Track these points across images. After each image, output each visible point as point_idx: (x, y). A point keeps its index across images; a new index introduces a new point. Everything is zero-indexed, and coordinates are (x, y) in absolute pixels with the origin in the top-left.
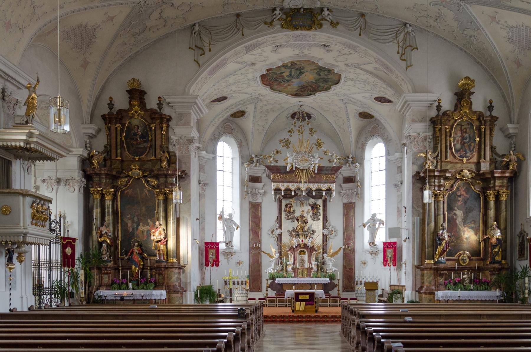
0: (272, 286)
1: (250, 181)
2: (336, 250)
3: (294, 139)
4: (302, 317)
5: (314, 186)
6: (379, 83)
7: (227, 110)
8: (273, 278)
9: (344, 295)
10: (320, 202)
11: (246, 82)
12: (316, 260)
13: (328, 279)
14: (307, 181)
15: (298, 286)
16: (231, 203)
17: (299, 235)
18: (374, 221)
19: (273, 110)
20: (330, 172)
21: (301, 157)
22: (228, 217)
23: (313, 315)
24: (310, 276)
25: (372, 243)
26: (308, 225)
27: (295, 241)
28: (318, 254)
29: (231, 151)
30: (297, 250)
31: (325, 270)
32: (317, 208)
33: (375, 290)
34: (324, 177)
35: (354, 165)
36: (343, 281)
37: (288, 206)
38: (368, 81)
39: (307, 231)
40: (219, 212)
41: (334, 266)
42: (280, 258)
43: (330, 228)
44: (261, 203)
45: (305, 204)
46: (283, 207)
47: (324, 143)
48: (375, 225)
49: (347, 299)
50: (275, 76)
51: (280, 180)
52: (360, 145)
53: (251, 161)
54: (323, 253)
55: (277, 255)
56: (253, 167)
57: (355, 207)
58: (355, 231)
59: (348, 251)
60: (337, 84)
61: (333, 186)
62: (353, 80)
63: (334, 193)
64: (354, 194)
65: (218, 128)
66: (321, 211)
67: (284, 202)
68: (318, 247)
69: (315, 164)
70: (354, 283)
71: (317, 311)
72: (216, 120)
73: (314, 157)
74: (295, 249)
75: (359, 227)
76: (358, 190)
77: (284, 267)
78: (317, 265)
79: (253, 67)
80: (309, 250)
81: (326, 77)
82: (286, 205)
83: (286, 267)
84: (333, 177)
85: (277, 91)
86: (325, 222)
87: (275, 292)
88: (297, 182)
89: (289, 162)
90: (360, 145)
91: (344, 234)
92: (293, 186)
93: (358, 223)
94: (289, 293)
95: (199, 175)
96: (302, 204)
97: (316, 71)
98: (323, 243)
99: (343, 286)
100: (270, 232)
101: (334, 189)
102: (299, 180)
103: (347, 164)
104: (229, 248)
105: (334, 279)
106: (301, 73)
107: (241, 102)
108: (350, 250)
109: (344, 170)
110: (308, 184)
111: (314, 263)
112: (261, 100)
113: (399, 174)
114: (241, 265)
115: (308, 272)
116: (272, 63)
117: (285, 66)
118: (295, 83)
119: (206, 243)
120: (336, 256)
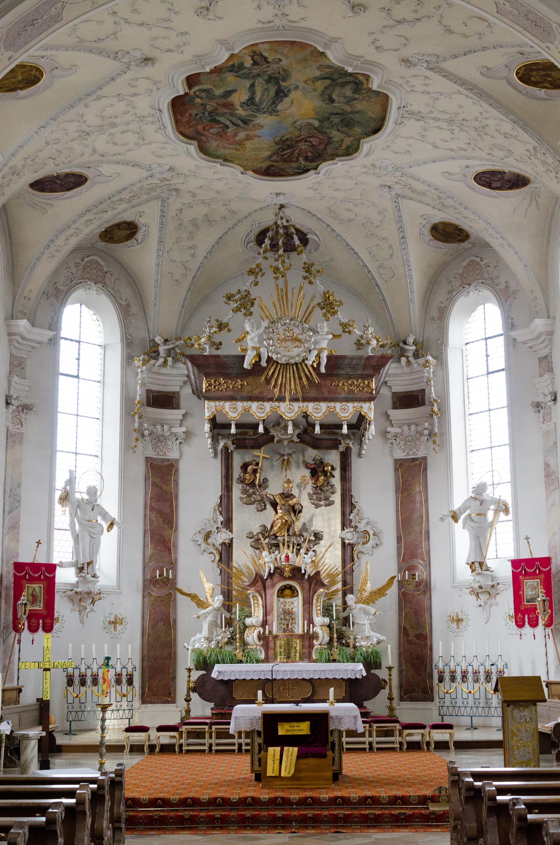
0: (204, 687)
1: (149, 405)
2: (380, 586)
3: (265, 292)
4: (286, 802)
5: (318, 411)
6: (495, 119)
7: (89, 216)
8: (205, 663)
9: (408, 712)
10: (333, 458)
11: (133, 127)
12: (327, 611)
13: (360, 666)
14: (300, 396)
15: (271, 688)
16: (98, 461)
17: (277, 546)
18: (482, 502)
19: (209, 221)
20: (359, 372)
21: (281, 332)
22: (86, 497)
23: (324, 795)
24: (311, 660)
25: (478, 565)
26: (303, 518)
27: (268, 561)
28: (330, 596)
29: (101, 329)
30: (273, 586)
31: (351, 641)
32: (325, 473)
33: (534, 703)
34: (344, 386)
35: (421, 361)
36: (401, 672)
37: (250, 468)
38: (461, 117)
39: (301, 535)
40: (60, 483)
41: (375, 628)
42: (228, 607)
43: (362, 527)
44: (177, 461)
45: (293, 464)
46: (237, 472)
47: (341, 303)
48: (485, 515)
49: (422, 727)
50: (211, 105)
52: (434, 312)
53: (152, 353)
54: (344, 595)
55: (218, 601)
56: (156, 369)
57: (425, 469)
59: (410, 589)
60: (376, 131)
61: (369, 409)
62: (419, 116)
63: (373, 427)
64: (422, 434)
65: (65, 263)
66: (336, 481)
67: (237, 461)
69: (321, 351)
70: (431, 676)
71: (336, 776)
72: (60, 241)
73: (315, 332)
74: (268, 583)
75: (442, 519)
76: (432, 424)
77: (236, 637)
79: (148, 70)
80: (306, 585)
81: (348, 109)
82: (245, 467)
83: (242, 633)
84: (368, 386)
85: (218, 157)
86: (348, 510)
87: (212, 705)
88: (271, 400)
89: (250, 344)
90: (434, 312)
92: (259, 411)
93: (436, 510)
94: (246, 715)
95: (9, 381)
96: (286, 464)
97: (321, 85)
98: (344, 566)
99: (401, 686)
101: (371, 415)
102: (277, 390)
103: (403, 360)
104: (84, 580)
105: (378, 666)
106: (281, 94)
107: (125, 195)
108: (418, 584)
109: (394, 375)
110: (301, 404)
111: (319, 620)
112: (177, 190)
113: (547, 376)
114: (119, 627)
115: (303, 647)
116: (199, 57)
117: (233, 67)
118: (266, 130)
119: (18, 566)
120: (381, 601)
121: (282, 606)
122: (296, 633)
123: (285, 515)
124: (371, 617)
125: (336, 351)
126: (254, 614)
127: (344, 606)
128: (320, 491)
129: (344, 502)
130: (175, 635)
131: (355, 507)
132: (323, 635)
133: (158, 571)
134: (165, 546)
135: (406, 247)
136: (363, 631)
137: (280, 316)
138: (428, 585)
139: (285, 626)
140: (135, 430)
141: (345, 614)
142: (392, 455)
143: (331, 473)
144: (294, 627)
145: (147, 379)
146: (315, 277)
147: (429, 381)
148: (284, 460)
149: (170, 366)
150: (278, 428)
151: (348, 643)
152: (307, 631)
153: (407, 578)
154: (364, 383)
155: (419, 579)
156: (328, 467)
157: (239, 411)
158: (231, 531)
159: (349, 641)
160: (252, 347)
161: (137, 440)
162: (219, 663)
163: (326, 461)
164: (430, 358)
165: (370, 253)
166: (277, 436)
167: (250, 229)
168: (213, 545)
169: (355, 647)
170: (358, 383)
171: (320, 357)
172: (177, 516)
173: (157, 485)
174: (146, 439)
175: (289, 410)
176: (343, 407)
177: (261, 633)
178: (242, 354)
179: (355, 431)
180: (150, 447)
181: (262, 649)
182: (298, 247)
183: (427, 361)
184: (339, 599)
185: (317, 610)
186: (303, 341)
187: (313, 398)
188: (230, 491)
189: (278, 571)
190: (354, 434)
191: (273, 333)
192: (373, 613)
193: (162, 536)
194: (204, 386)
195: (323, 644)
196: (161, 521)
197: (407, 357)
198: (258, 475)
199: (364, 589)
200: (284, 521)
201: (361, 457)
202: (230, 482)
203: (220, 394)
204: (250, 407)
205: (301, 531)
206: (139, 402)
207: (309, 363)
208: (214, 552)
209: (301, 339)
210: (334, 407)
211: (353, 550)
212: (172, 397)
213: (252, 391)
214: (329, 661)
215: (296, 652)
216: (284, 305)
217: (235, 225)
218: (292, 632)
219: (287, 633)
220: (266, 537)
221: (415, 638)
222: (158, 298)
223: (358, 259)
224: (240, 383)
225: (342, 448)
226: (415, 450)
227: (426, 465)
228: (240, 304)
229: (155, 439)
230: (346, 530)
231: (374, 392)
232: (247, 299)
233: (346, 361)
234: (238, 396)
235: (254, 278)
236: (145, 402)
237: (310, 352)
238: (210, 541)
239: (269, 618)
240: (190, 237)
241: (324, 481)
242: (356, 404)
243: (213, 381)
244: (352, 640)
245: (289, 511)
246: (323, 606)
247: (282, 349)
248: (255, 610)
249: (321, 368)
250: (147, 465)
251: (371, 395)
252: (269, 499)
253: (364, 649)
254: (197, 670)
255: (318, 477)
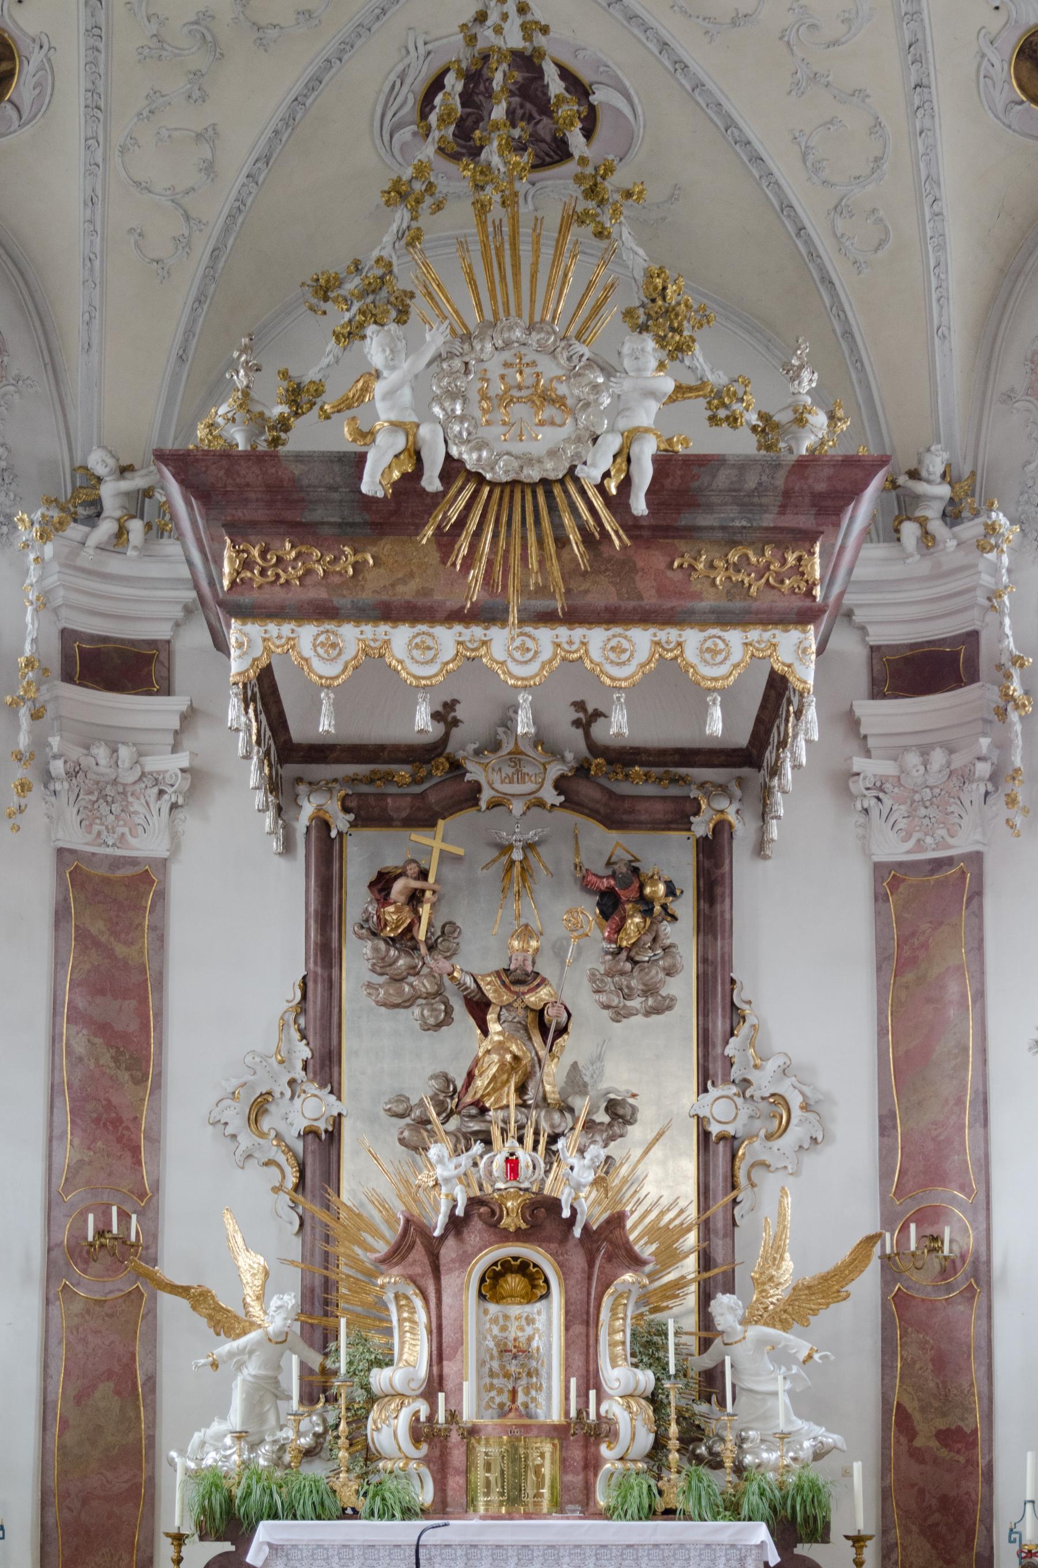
1: (68, 677)
10: (670, 859)
12: (647, 1348)
13: (760, 1533)
20: (768, 520)
21: (494, 367)
24: (587, 1508)
26: (573, 1048)
27: (446, 1177)
30: (465, 1260)
31: (728, 1452)
32: (646, 906)
34: (711, 571)
35: (970, 530)
37: (399, 887)
43: (764, 1082)
44: (163, 864)
46: (357, 900)
51: (298, 594)
54: (705, 1298)
55: (278, 1312)
56: (88, 556)
57: (978, 893)
58: (983, 1101)
59: (921, 1281)
66: (682, 934)
67: (362, 856)
68: (655, 1232)
69: (631, 436)
74: (449, 1251)
76: (1003, 746)
78: (655, 1400)
80: (577, 1260)
82: (382, 884)
84: (798, 570)
86: (719, 1025)
91: (886, 1125)
100: (235, 1116)
101: (806, 674)
103: (910, 531)
108: (949, 1267)
109: (875, 585)
111: (620, 1376)
115: (564, 1465)
121: (496, 1330)
122: (542, 1418)
123: (511, 1038)
124: (795, 1369)
125: (685, 442)
126: (401, 1354)
127: (703, 1334)
128: (628, 966)
129: (706, 1003)
130: (152, 1424)
131: (744, 1018)
132: (632, 1428)
133: (91, 1217)
134: (119, 1140)
135: (927, 123)
136: (767, 1417)
137: (489, 316)
138: (983, 1268)
139: (505, 1398)
140: (19, 757)
141: (707, 1361)
142: (866, 852)
143: (664, 907)
144: (534, 1400)
145: (61, 592)
146: (616, 213)
147: (993, 596)
148: (512, 863)
149: (135, 548)
150: (493, 759)
151: (718, 1454)
152: (579, 1412)
153: (913, 1246)
154: (784, 561)
155: (951, 1251)
156: (654, 884)
157: (347, 656)
158: (336, 1092)
159: (718, 1448)
160: (392, 424)
161: (24, 787)
162: (275, 1517)
163: (647, 869)
164: (1000, 518)
165: (804, 156)
166: (490, 785)
167: (400, 68)
168: (278, 1136)
169: (739, 1469)
170: (763, 561)
171: (629, 460)
172: (160, 1044)
173: (97, 944)
174: (58, 786)
175: (521, 658)
176: (709, 644)
177: (423, 1419)
178: (357, 447)
179: (745, 771)
180: (71, 814)
181: (425, 1471)
182: (557, 105)
183: (992, 529)
184: (688, 1313)
185: (613, 1344)
186: (569, 402)
187: (607, 609)
188: (335, 961)
189: (481, 1213)
190: (740, 781)
191: (467, 372)
192: (803, 1355)
193: (109, 1106)
194: (226, 569)
195: (630, 1456)
196: (106, 1059)
197: (922, 522)
198: (425, 911)
199: (771, 1278)
200: (508, 1057)
201: (766, 857)
202: (335, 935)
203: (277, 595)
204: (387, 642)
205: (564, 1094)
206: (29, 663)
207: (590, 475)
208: (281, 1159)
209: (564, 397)
210: (680, 644)
211: (734, 1156)
212: (148, 659)
213: (393, 585)
214: (651, 1513)
215: (540, 1485)
216: (503, 278)
217: (347, 46)
218: (529, 1416)
219: (511, 1420)
220: (451, 1113)
221: (934, 1444)
222: (96, 322)
223: (764, 183)
224: (352, 559)
225: (701, 826)
226: (942, 832)
227: (979, 878)
228: (362, 312)
229: (91, 793)
230: (713, 1092)
231: (818, 592)
232: (384, 293)
233: (723, 478)
234: (343, 601)
235: (407, 216)
236: (55, 665)
237: (595, 440)
238: (266, 1124)
239: (449, 1367)
240: (196, 94)
241: (641, 931)
242: (754, 634)
243: (256, 552)
244: (729, 1445)
245: (526, 1029)
246: (634, 1334)
247: (497, 430)
248: (402, 1343)
249: (632, 501)
250: (60, 875)
251: (808, 603)
252: (460, 985)
253: (771, 1475)
254: (202, 1538)
255: (623, 920)
